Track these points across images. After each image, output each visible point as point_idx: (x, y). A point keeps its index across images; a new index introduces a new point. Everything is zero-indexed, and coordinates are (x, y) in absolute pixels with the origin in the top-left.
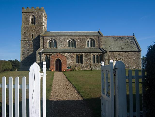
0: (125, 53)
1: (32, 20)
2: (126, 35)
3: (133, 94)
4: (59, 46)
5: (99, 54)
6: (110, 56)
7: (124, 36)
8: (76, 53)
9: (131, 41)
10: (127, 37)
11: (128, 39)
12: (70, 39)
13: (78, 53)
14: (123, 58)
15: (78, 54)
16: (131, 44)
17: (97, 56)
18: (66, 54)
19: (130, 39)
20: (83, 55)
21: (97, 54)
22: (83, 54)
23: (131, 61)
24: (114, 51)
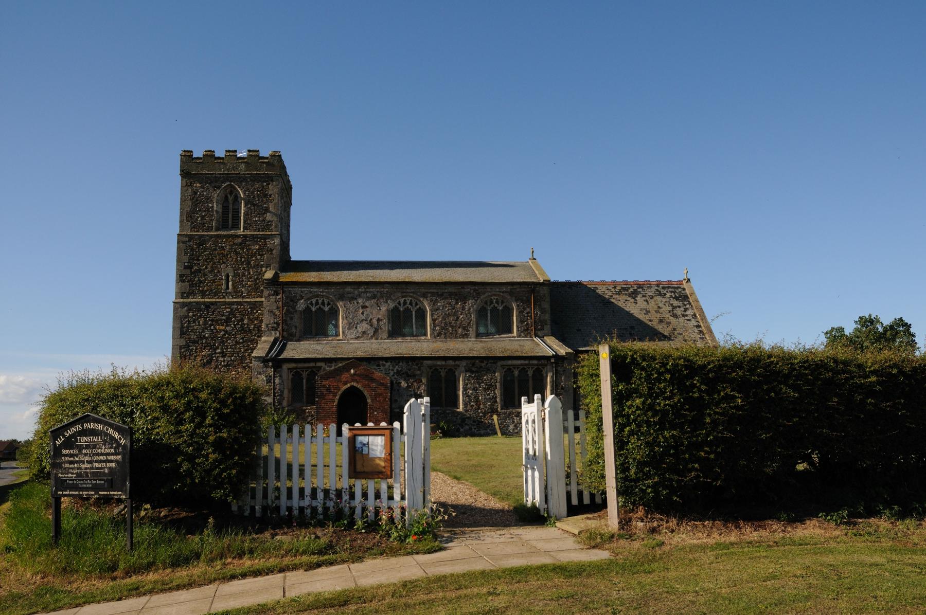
1: (225, 209)
7: (641, 279)
8: (429, 362)
9: (674, 308)
11: (660, 294)
12: (403, 297)
13: (439, 363)
16: (675, 316)
19: (668, 295)
22: (464, 363)
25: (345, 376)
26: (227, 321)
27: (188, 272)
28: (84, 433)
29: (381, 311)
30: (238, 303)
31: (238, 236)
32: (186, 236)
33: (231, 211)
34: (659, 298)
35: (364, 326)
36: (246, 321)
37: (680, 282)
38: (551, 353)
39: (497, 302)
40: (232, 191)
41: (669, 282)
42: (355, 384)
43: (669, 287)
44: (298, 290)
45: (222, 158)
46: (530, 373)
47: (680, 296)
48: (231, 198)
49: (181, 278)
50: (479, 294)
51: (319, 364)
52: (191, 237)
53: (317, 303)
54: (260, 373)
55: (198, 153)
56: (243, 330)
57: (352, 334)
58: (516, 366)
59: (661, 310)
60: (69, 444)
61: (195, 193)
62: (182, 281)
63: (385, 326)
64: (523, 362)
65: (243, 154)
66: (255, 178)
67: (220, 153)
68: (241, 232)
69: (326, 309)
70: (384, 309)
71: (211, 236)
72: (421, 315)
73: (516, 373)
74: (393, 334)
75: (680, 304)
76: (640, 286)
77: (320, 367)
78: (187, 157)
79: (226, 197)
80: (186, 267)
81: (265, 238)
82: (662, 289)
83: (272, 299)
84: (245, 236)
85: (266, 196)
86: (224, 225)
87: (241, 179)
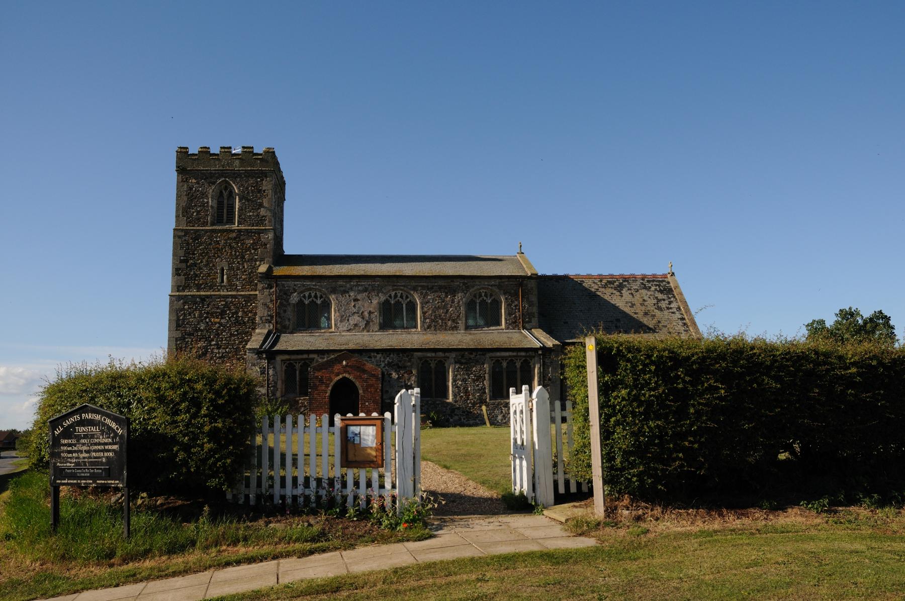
1: (220, 204)
2: (638, 272)
3: (61, 488)
7: (627, 272)
8: (419, 354)
9: (659, 300)
10: (643, 279)
11: (645, 288)
12: (393, 290)
13: (429, 355)
15: (295, 360)
16: (660, 309)
17: (511, 362)
18: (375, 357)
19: (653, 288)
21: (302, 359)
22: (453, 355)
25: (337, 368)
26: (222, 314)
27: (184, 266)
28: (82, 423)
29: (372, 304)
30: (232, 296)
31: (233, 231)
32: (182, 230)
33: (226, 205)
34: (644, 292)
35: (356, 319)
36: (240, 314)
37: (665, 276)
38: (538, 345)
39: (486, 296)
40: (227, 186)
41: (654, 276)
42: (347, 375)
43: (653, 281)
44: (291, 283)
45: (217, 155)
46: (518, 365)
47: (665, 290)
48: (225, 194)
49: (177, 272)
50: (468, 288)
51: (311, 356)
52: (186, 232)
53: (310, 296)
54: (254, 365)
55: (194, 150)
56: (238, 322)
57: (344, 326)
58: (504, 358)
59: (646, 303)
60: (67, 433)
61: (191, 189)
62: (178, 275)
63: (377, 318)
64: (511, 354)
65: (237, 150)
66: (249, 174)
67: (215, 150)
68: (235, 226)
69: (319, 302)
70: (375, 302)
71: (206, 231)
72: (412, 307)
73: (505, 364)
74: (384, 327)
75: (665, 297)
76: (626, 279)
77: (313, 359)
78: (183, 153)
79: (221, 192)
80: (181, 261)
81: (259, 232)
82: (647, 282)
83: (266, 292)
84: (240, 231)
85: (259, 191)
86: (219, 220)
87: (235, 175)
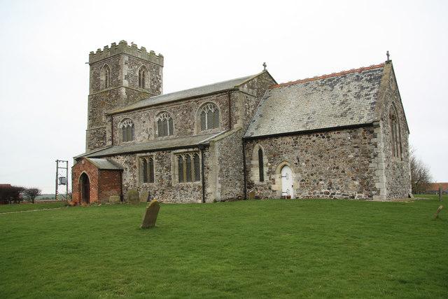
0: (315, 138)
4: (140, 135)
5: (191, 152)
6: (264, 154)
14: (308, 156)
20: (154, 159)
21: (185, 152)
22: (154, 154)
23: (337, 168)
24: (277, 136)
37: (382, 66)
49: (90, 118)
75: (370, 85)
76: (344, 74)
